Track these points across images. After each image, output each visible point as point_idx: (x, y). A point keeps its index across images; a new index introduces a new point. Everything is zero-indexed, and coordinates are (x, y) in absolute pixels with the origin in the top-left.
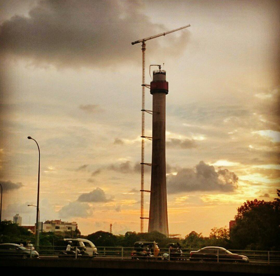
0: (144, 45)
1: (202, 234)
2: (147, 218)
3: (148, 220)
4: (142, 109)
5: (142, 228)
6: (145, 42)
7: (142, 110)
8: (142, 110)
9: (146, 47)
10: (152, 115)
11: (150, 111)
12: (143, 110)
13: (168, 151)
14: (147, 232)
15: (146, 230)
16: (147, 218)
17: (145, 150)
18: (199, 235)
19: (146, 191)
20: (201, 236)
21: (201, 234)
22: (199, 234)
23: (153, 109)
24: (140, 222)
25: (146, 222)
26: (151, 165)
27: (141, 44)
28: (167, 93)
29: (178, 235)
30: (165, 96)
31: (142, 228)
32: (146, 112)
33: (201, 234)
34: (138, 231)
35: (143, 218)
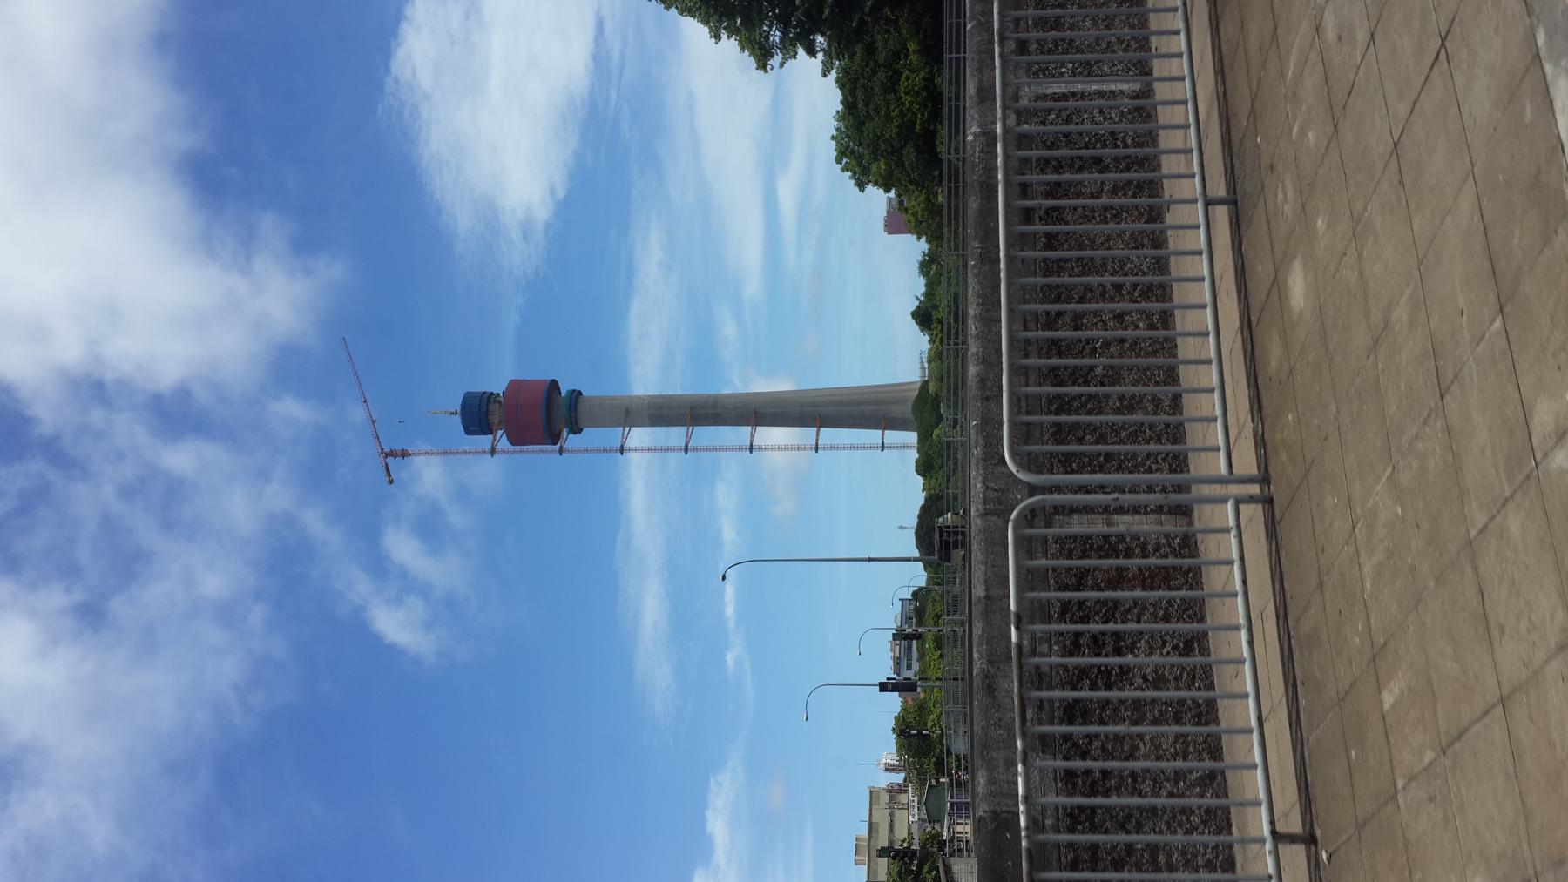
0: (392, 454)
1: (919, 295)
2: (883, 434)
3: (887, 432)
4: (684, 453)
5: (906, 447)
6: (387, 450)
7: (751, 452)
8: (751, 452)
9: (399, 448)
10: (695, 428)
11: (623, 434)
12: (686, 450)
13: (1194, 366)
14: (915, 434)
15: (912, 437)
16: (883, 434)
17: (782, 442)
18: (920, 301)
19: (817, 440)
20: (922, 298)
21: (917, 298)
22: (917, 303)
23: (618, 425)
24: (895, 452)
25: (893, 436)
26: (627, 429)
27: (390, 459)
28: (580, 393)
29: (921, 358)
30: (586, 397)
31: (906, 447)
32: (689, 442)
33: (917, 298)
34: (914, 455)
35: (751, 445)
